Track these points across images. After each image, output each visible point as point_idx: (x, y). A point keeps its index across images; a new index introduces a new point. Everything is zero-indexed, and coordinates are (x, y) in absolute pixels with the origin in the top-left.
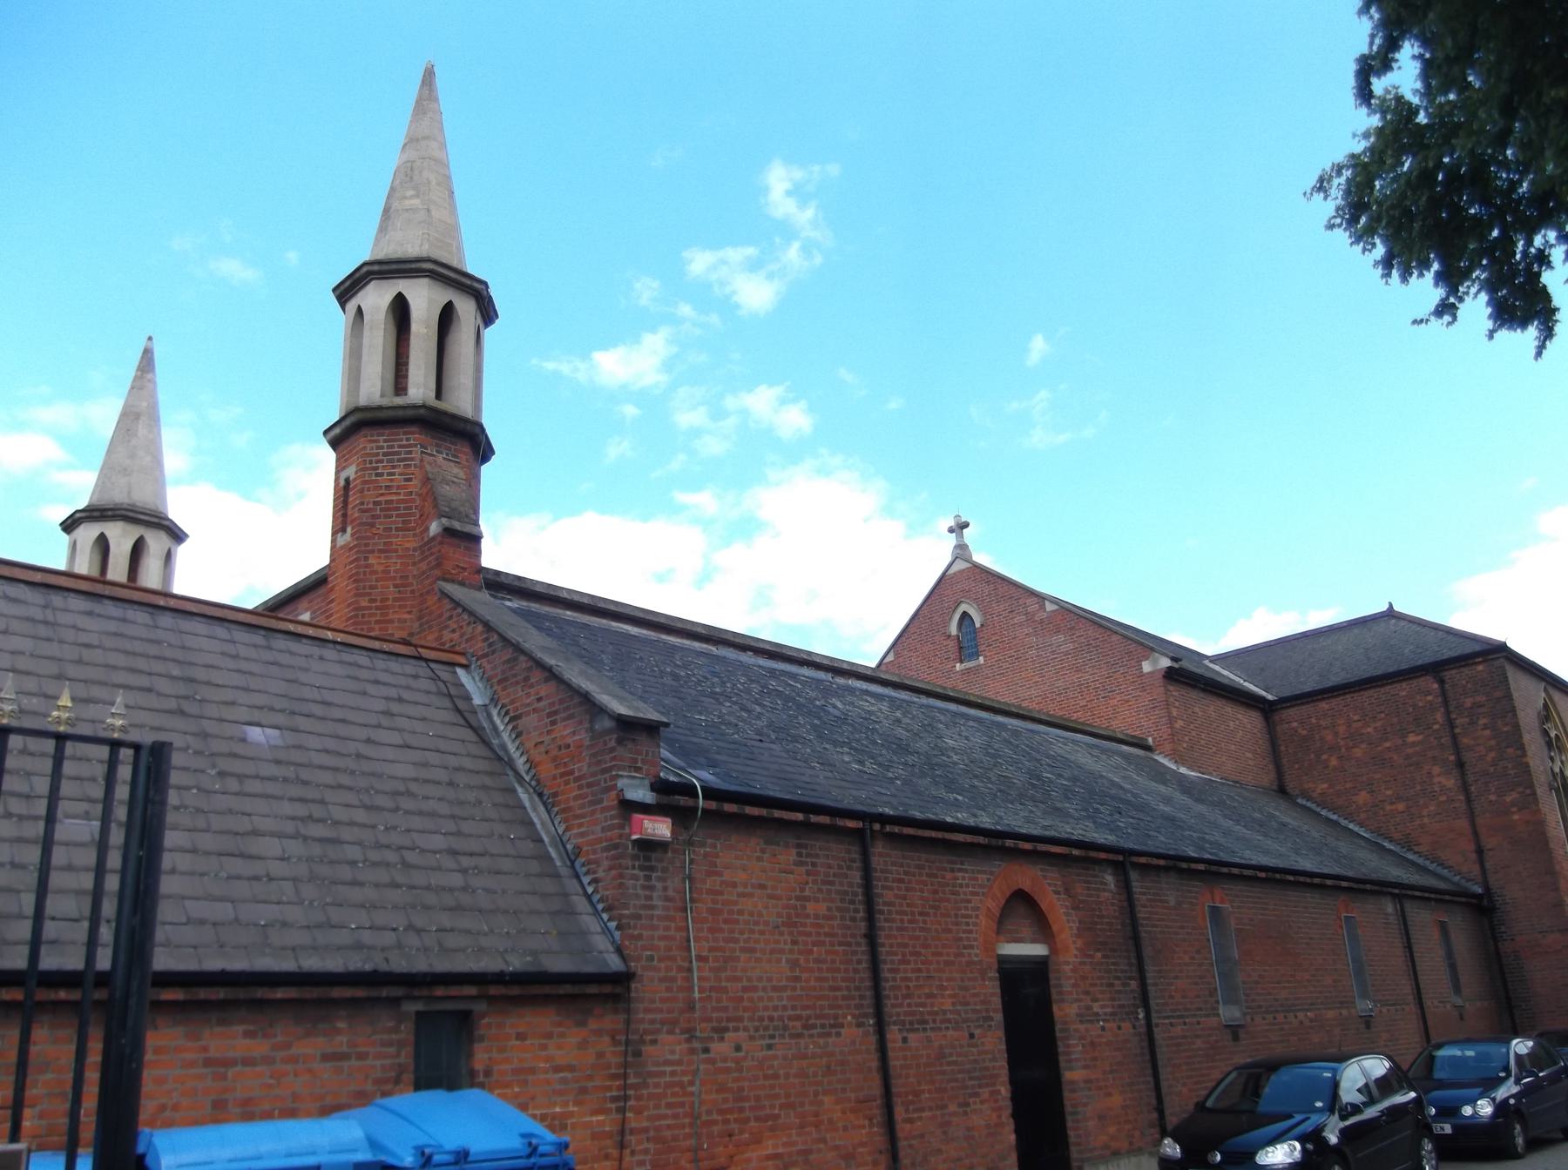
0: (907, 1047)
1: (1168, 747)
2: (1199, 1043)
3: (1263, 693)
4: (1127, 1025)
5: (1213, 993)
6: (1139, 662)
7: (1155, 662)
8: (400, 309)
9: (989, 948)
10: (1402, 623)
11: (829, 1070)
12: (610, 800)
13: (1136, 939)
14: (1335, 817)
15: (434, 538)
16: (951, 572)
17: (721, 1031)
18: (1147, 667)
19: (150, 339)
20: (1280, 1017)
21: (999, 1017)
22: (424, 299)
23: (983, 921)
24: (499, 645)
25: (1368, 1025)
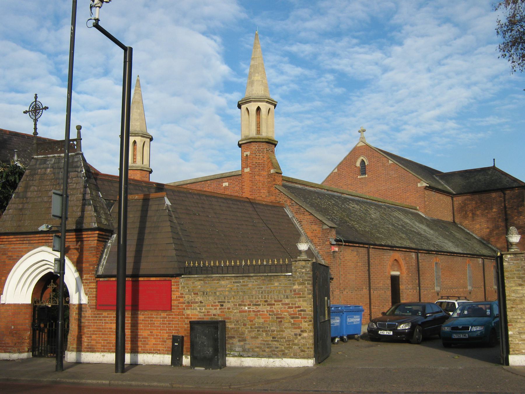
0: (374, 293)
1: (423, 210)
2: (430, 295)
3: (452, 191)
4: (415, 291)
5: (434, 284)
6: (417, 183)
7: (422, 184)
8: (259, 109)
9: (389, 273)
10: (497, 172)
11: (361, 298)
12: (327, 243)
13: (418, 271)
14: (469, 231)
15: (272, 174)
16: (358, 146)
17: (345, 289)
18: (419, 185)
19: (138, 76)
20: (449, 290)
21: (390, 288)
22: (264, 107)
23: (388, 266)
24: (295, 204)
25: (470, 293)
